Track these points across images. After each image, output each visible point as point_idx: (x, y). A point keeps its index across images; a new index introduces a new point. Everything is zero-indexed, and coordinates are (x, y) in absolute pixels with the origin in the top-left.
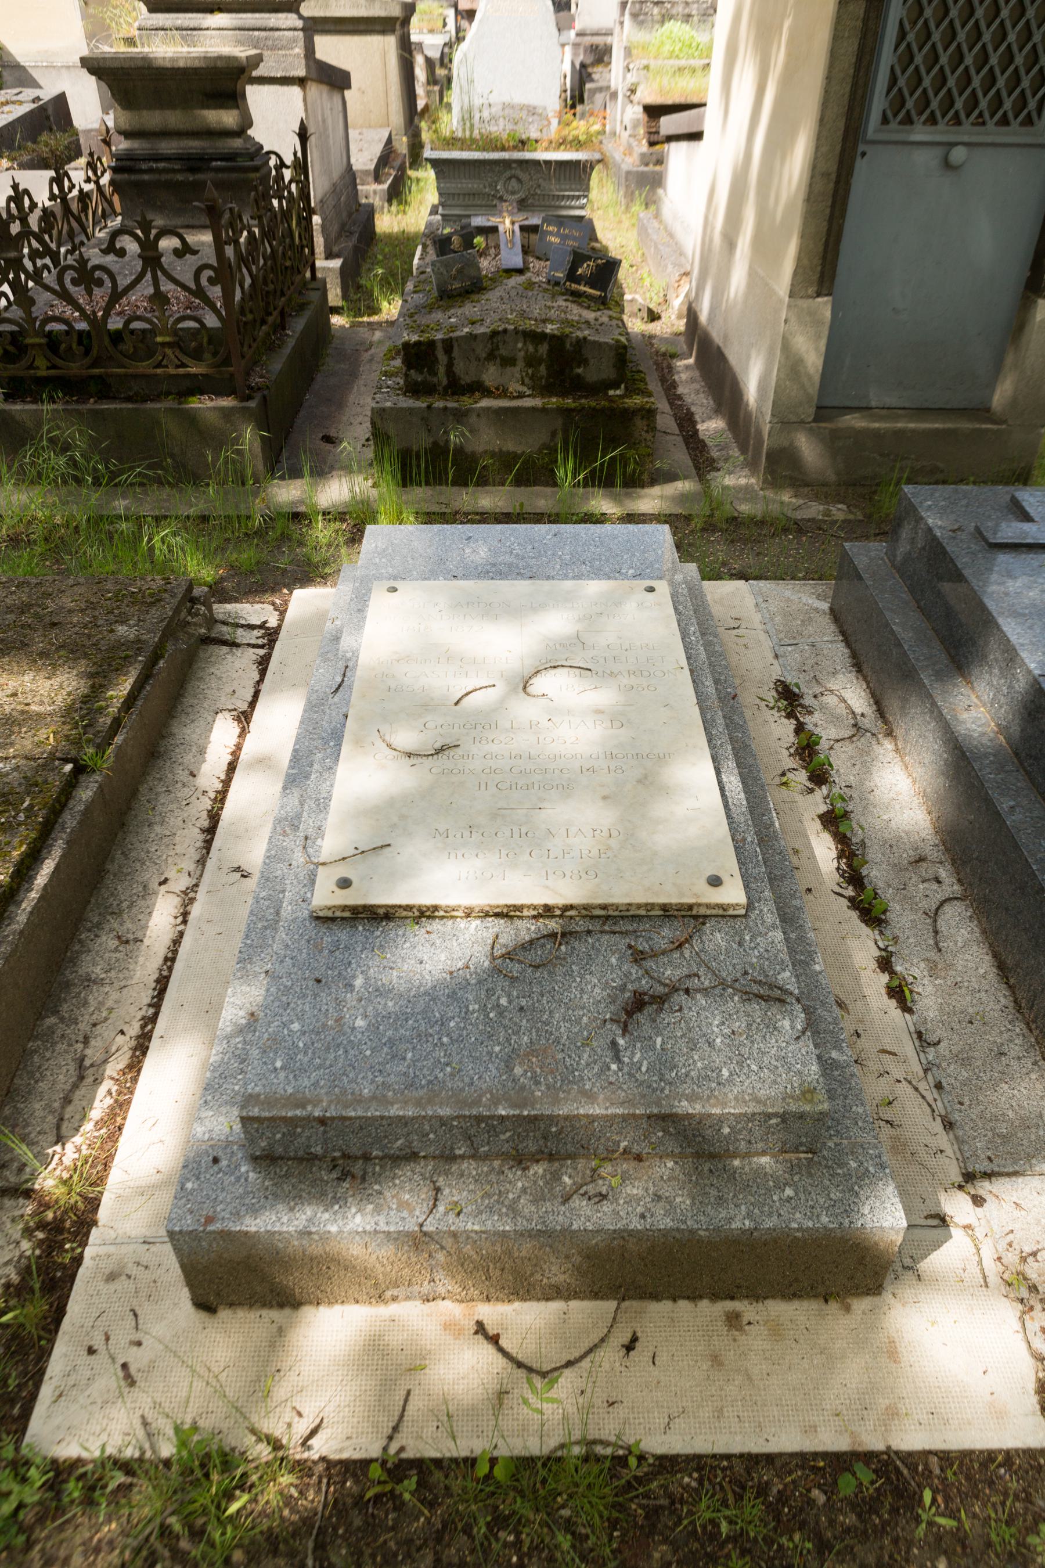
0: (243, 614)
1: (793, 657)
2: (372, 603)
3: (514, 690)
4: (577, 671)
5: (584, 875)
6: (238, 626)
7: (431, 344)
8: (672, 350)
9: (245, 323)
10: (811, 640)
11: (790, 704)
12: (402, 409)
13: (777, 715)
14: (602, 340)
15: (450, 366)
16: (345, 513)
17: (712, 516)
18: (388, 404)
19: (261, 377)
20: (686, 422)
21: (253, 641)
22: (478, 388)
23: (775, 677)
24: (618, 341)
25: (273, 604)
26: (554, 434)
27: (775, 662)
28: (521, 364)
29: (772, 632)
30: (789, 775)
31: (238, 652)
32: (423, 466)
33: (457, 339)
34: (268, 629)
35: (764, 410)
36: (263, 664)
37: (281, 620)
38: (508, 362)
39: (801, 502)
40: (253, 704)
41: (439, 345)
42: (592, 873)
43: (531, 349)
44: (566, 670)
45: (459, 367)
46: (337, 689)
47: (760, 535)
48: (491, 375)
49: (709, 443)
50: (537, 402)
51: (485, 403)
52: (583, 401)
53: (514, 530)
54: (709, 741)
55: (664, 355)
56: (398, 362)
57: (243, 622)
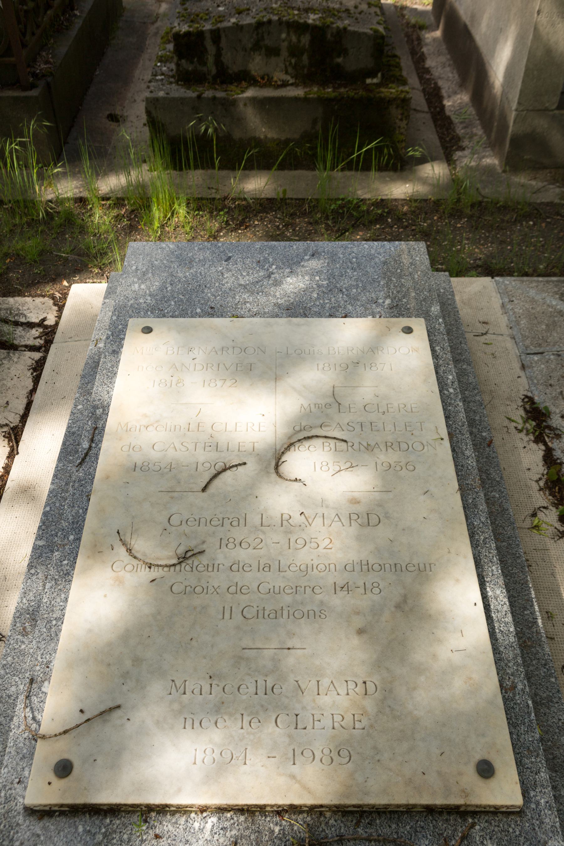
0: (24, 309)
1: (540, 367)
2: (127, 343)
3: (266, 470)
4: (332, 442)
5: (336, 757)
6: (17, 324)
7: (200, 34)
8: (421, 21)
9: (26, 12)
10: (556, 348)
11: (538, 426)
12: (174, 99)
13: (526, 439)
14: (361, 30)
15: (218, 55)
16: (123, 199)
17: (459, 200)
18: (161, 94)
19: (47, 62)
20: (434, 96)
21: (31, 342)
22: (245, 78)
23: (523, 392)
24: (376, 31)
25: (53, 297)
26: (315, 122)
27: (522, 374)
28: (284, 53)
29: (519, 337)
30: (540, 515)
31: (15, 356)
32: (191, 155)
33: (225, 29)
34: (46, 327)
35: (510, 97)
36: (38, 368)
37: (59, 317)
38: (273, 52)
39: (540, 184)
40: (24, 418)
41: (208, 36)
42: (344, 753)
43: (294, 39)
44: (320, 441)
45: (227, 57)
46: (83, 460)
47: (503, 221)
48: (257, 65)
49: (455, 119)
50: (298, 92)
51: (250, 93)
52: (342, 90)
53: (272, 248)
54: (472, 536)
55: (414, 26)
56: (171, 47)
57: (23, 320)
